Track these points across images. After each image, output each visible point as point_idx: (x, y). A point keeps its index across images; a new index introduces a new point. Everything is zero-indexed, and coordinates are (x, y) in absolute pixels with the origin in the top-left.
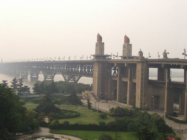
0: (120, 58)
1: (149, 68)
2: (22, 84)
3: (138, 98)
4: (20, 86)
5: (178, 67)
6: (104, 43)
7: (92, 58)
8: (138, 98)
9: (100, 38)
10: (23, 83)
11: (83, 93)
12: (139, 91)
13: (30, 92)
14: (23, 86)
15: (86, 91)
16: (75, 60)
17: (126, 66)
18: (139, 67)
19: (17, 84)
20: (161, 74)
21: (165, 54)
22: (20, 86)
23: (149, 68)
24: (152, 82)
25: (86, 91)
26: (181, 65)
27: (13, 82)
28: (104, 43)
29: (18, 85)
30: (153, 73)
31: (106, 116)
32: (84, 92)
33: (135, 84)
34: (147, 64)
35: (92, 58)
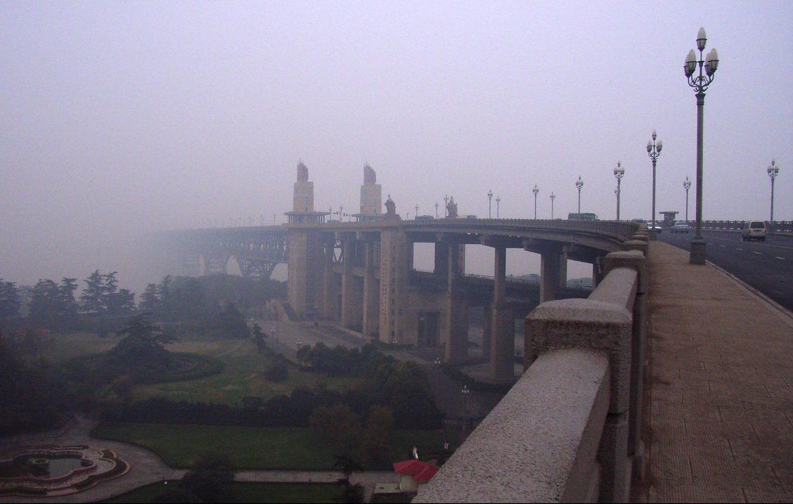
0: (354, 219)
1: (508, 250)
2: (114, 287)
3: (386, 318)
4: (109, 289)
5: (474, 240)
6: (312, 183)
7: (285, 220)
8: (386, 318)
9: (303, 171)
10: (115, 284)
11: (267, 304)
12: (385, 302)
13: (133, 303)
14: (117, 291)
15: (273, 300)
16: (494, 217)
17: (358, 238)
18: (386, 240)
19: (101, 286)
20: (440, 257)
21: (452, 208)
22: (109, 289)
23: (508, 250)
24: (418, 279)
25: (273, 300)
26: (482, 235)
27: (90, 280)
28: (312, 183)
29: (104, 288)
30: (424, 257)
31: (638, 226)
32: (270, 301)
33: (378, 281)
34: (406, 232)
35: (285, 220)
